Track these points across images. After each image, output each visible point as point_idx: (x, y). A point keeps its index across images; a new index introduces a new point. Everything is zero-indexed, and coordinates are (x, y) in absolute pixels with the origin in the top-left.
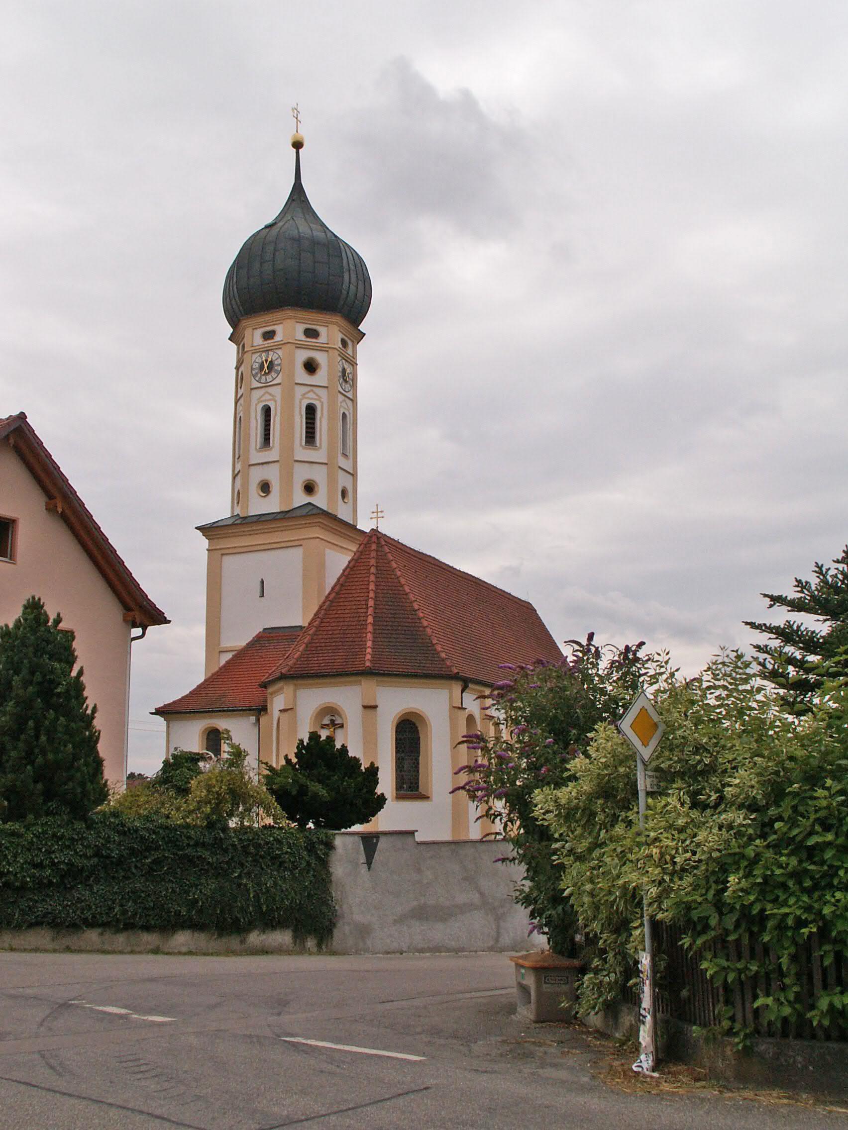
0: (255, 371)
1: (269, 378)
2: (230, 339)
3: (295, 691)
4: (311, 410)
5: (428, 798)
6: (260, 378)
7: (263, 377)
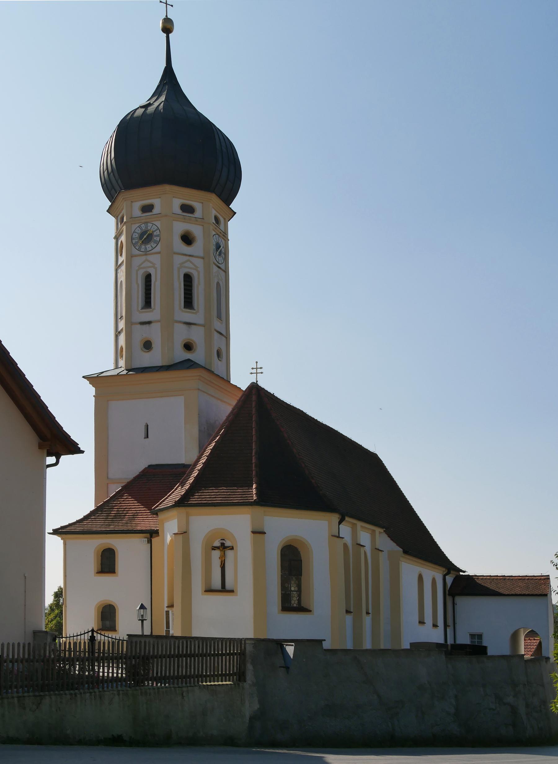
0: (138, 240)
1: (149, 247)
2: (108, 211)
3: (188, 515)
4: (188, 279)
5: (310, 611)
6: (140, 247)
7: (143, 247)
